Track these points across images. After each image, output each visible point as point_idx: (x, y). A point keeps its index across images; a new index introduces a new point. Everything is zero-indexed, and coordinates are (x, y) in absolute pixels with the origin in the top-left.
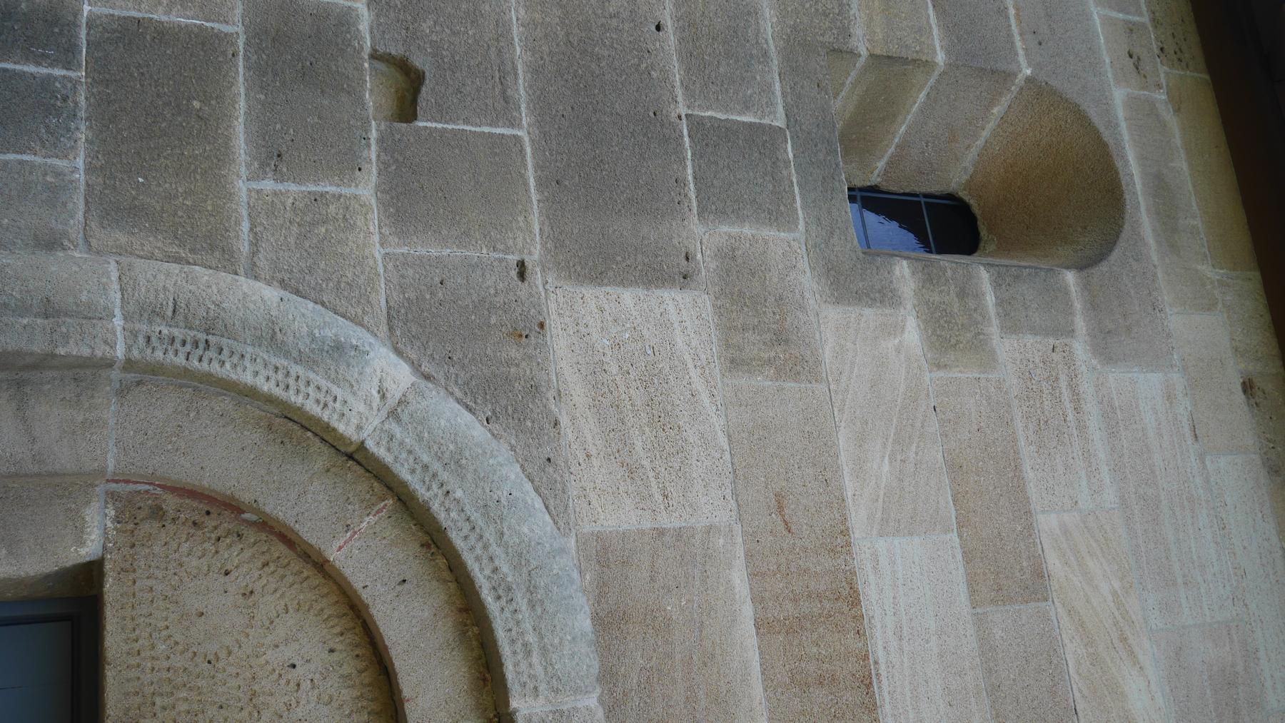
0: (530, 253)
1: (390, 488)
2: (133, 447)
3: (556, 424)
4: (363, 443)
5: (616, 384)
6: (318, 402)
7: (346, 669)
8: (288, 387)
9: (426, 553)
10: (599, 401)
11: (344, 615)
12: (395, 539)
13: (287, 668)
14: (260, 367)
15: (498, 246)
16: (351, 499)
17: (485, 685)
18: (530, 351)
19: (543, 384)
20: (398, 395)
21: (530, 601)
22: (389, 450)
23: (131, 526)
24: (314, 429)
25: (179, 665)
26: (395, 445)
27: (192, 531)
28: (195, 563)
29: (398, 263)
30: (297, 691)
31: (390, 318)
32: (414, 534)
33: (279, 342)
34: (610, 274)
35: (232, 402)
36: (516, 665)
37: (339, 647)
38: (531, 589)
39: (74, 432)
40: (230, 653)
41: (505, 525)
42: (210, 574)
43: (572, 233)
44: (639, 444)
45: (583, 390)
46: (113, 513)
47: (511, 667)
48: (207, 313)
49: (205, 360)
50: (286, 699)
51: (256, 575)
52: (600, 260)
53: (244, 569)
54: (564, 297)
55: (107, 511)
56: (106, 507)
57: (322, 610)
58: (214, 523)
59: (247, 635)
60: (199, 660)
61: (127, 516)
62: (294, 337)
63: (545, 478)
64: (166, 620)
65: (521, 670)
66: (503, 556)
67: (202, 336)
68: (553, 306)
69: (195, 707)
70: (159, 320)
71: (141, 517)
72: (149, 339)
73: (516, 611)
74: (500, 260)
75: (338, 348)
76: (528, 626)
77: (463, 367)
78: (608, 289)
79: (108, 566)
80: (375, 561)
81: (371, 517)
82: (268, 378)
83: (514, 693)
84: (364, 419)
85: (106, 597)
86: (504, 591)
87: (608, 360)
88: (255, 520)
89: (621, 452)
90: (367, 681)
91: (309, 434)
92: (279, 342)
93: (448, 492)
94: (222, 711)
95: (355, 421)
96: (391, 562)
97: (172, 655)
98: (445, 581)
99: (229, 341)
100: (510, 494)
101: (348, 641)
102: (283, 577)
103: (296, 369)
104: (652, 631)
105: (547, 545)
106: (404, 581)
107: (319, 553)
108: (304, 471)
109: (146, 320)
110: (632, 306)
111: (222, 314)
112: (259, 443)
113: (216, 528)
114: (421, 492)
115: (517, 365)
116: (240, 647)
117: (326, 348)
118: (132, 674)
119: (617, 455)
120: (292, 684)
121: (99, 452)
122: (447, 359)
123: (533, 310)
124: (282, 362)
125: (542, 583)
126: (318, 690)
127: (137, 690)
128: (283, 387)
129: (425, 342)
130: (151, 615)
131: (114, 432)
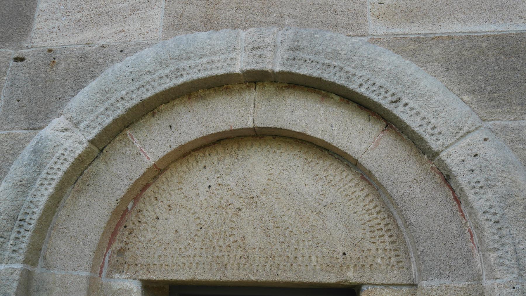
0: (10, 54)
1: (121, 131)
2: (78, 262)
3: (103, 46)
4: (89, 141)
5: (88, 15)
6: (63, 164)
7: (215, 161)
8: (52, 179)
9: (157, 114)
10: (95, 24)
11: (188, 160)
12: (147, 130)
13: (210, 190)
14: (39, 193)
15: (4, 71)
16: (124, 151)
17: (229, 88)
18: (62, 57)
19: (81, 52)
20: (67, 122)
21: (186, 59)
22: (94, 128)
23: (126, 266)
24: (83, 169)
25: (200, 244)
26: (92, 124)
27: (133, 235)
28: (150, 234)
29: (5, 123)
30: (222, 185)
31: (34, 129)
32: (147, 120)
33: (27, 182)
34: (28, 14)
35: (63, 210)
36: (218, 68)
37: (204, 163)
38: (180, 58)
39: (65, 292)
40: (198, 218)
41: (144, 70)
42: (157, 226)
43: (3, 32)
44: (121, 5)
45: (88, 32)
46: (118, 274)
47: (219, 71)
48: (5, 220)
49: (30, 221)
50: (225, 191)
51: (161, 203)
52: (20, 18)
53: (157, 210)
54: (36, 38)
55: (116, 277)
56: (114, 278)
57: (184, 171)
58: (131, 224)
59: (191, 209)
60: (199, 233)
61: (120, 267)
62: (25, 174)
63: (130, 54)
64: (177, 249)
65: (221, 66)
66: (160, 72)
67: (18, 222)
68: (41, 44)
69: (222, 236)
70: (5, 246)
71: (122, 260)
72: (14, 251)
73: (190, 67)
74: (12, 70)
75: (35, 152)
76: (199, 61)
77: (65, 92)
78: (36, 15)
79: (145, 278)
80: (158, 140)
81: (134, 142)
82: (46, 189)
83: (232, 70)
84: (76, 140)
85: (160, 279)
86: (178, 72)
87: (74, 18)
88: (132, 203)
89: (123, 15)
90: (223, 151)
91: (86, 171)
92: (27, 182)
93: (122, 98)
94: (227, 223)
95: (77, 145)
96: (159, 133)
97: (195, 247)
98: (173, 106)
99: (22, 208)
100: (129, 66)
101: (201, 159)
102: (164, 190)
103: (43, 175)
104: (218, 5)
105: (159, 49)
106: (170, 126)
107: (150, 169)
108: (105, 175)
109: (4, 252)
110: (47, 4)
111: (6, 212)
112: (87, 198)
113: (134, 223)
114: (120, 112)
115: (69, 64)
116: (196, 213)
117: (34, 158)
118: (201, 266)
119: (125, 17)
120: (218, 188)
121: (78, 280)
122: (60, 100)
123: (41, 55)
124: (38, 182)
125: (178, 52)
126: (223, 175)
127: (209, 264)
128: (52, 181)
129: (49, 111)
130: (173, 257)
131: (69, 272)
